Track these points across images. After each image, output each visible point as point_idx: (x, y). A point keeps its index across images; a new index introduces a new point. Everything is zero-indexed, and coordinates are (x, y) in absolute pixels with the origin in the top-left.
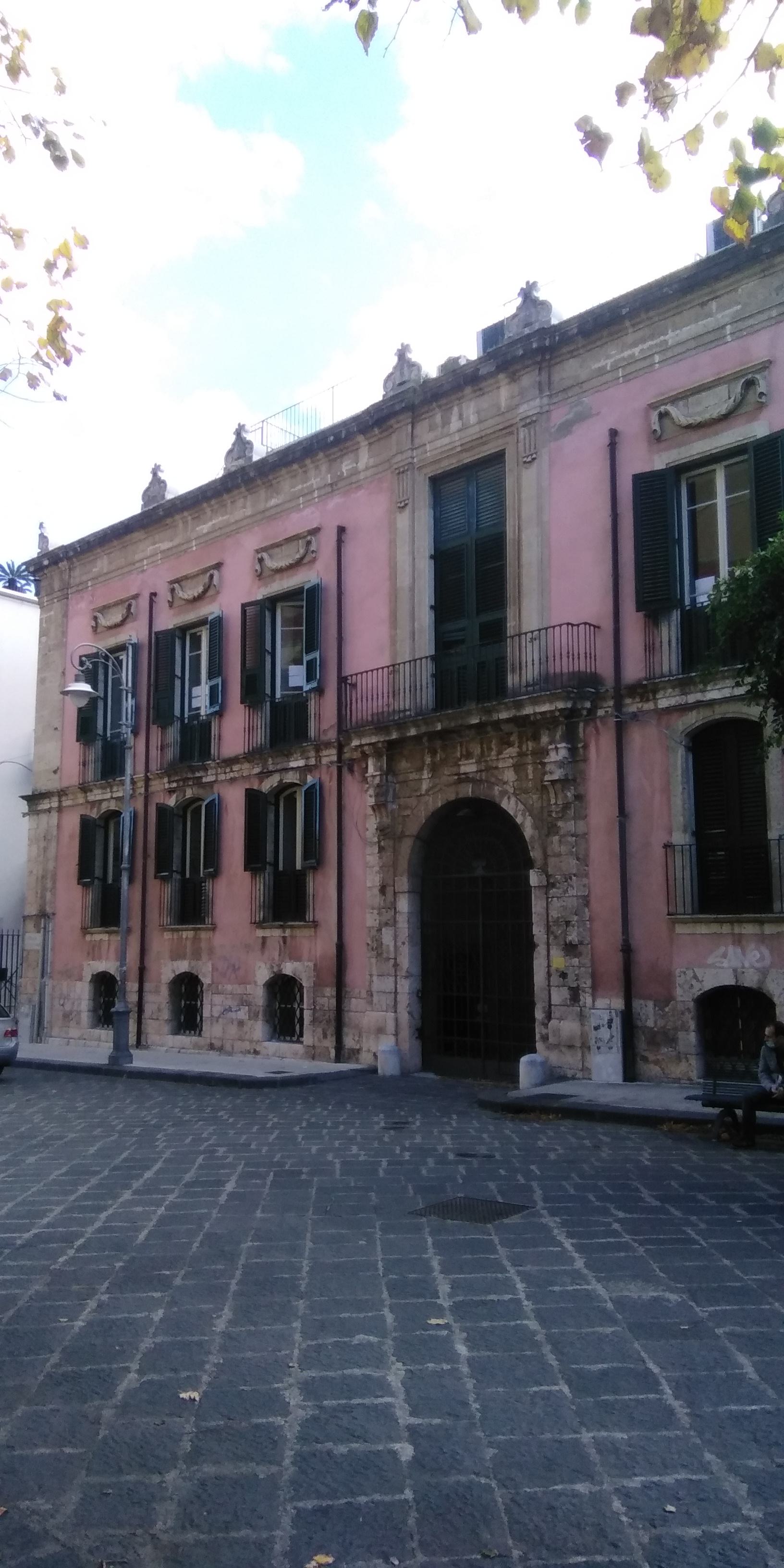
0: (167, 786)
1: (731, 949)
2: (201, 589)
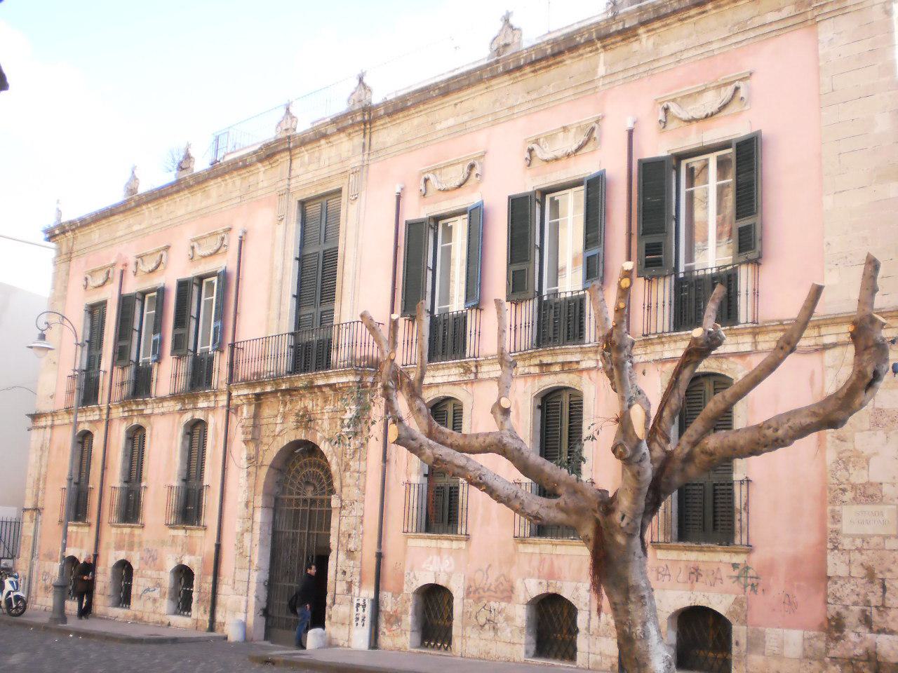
0: (121, 415)
1: (435, 557)
2: (154, 265)
